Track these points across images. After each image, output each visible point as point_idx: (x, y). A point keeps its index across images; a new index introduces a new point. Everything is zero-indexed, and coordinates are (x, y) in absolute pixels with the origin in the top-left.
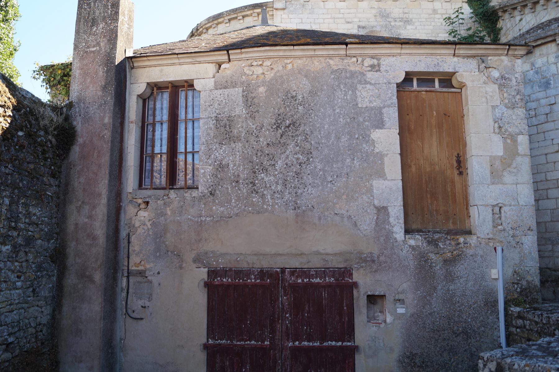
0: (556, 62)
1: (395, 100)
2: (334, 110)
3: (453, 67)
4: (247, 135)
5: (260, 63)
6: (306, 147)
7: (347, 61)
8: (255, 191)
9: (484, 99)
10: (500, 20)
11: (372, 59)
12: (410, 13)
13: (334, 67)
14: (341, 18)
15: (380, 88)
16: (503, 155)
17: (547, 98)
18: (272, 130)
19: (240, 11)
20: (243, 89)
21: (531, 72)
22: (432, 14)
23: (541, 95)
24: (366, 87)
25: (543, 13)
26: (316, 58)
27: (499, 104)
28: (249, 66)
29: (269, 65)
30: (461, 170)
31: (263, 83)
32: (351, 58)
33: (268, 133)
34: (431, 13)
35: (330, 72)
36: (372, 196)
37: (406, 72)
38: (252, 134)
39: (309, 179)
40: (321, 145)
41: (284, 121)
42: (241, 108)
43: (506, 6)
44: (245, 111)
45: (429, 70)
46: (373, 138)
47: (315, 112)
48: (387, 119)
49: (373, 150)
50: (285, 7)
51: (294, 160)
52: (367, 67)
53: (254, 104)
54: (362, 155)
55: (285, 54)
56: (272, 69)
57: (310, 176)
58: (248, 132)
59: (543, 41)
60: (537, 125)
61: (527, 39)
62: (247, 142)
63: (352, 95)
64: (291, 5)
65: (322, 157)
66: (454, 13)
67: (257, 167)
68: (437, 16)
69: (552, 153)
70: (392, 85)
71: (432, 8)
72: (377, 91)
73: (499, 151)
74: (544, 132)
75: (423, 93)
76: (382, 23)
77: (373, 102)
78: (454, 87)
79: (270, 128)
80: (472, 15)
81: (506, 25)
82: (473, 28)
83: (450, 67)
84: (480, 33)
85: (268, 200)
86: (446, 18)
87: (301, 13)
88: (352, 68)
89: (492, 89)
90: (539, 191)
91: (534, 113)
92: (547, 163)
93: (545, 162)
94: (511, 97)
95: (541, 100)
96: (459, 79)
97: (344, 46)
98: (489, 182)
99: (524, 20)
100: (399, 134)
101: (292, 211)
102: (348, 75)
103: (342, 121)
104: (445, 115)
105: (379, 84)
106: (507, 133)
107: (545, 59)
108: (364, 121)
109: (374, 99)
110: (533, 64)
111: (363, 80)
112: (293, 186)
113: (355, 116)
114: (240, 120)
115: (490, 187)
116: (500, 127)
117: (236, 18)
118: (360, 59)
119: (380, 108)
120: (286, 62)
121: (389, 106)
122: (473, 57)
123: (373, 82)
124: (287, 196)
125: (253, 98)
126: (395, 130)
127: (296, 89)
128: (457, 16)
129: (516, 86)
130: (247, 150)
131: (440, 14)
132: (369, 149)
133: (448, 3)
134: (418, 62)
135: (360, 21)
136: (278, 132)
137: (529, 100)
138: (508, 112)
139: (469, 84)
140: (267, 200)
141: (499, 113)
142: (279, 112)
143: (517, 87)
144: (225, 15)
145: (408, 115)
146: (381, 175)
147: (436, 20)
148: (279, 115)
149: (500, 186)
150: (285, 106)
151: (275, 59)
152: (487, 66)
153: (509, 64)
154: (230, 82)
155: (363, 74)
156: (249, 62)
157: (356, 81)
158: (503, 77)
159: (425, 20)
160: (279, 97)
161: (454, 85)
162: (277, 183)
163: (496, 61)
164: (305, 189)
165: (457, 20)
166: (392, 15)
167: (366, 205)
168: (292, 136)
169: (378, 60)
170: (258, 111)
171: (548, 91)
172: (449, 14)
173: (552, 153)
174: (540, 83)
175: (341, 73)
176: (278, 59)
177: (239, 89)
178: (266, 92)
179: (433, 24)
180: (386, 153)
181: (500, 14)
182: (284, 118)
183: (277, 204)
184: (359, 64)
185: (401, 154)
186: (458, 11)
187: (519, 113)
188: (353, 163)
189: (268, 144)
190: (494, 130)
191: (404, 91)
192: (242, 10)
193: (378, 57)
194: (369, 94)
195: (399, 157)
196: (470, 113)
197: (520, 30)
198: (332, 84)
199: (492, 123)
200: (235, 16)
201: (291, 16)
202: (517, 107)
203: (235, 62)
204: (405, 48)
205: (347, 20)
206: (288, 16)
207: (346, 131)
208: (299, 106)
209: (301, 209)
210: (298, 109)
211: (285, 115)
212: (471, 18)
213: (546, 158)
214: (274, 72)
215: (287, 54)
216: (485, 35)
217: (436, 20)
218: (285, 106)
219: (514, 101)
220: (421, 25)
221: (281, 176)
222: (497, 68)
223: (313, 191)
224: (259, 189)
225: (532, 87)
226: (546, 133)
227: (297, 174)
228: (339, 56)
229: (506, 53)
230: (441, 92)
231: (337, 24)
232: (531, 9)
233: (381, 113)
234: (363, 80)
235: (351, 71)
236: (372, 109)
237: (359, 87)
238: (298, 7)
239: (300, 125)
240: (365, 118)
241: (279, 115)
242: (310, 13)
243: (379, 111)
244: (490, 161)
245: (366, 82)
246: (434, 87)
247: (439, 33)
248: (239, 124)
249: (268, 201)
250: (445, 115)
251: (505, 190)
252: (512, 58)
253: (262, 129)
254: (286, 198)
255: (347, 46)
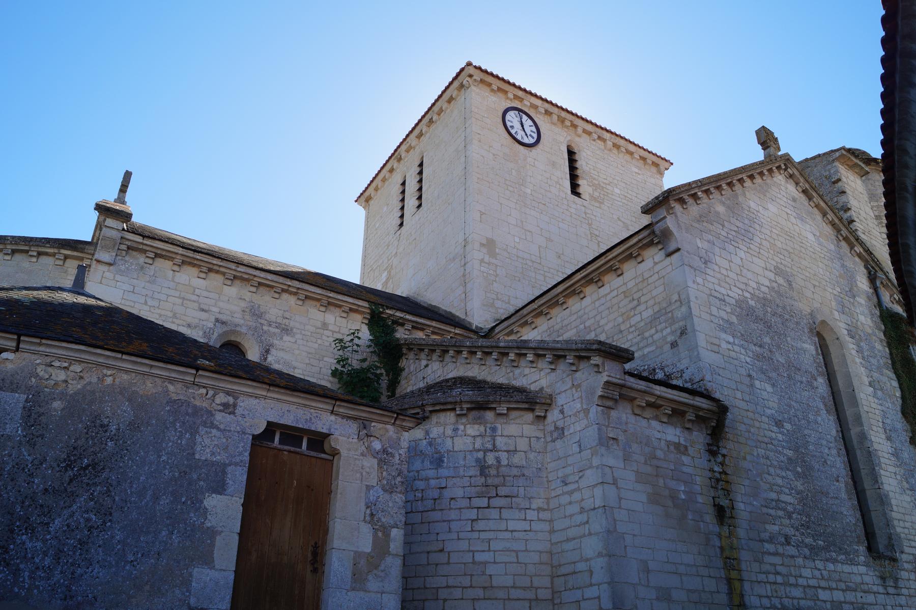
0: (453, 435)
1: (246, 457)
2: (160, 457)
3: (328, 427)
4: (15, 469)
5: (66, 365)
6: (105, 503)
7: (192, 391)
8: (5, 562)
9: (358, 475)
10: (403, 358)
11: (228, 396)
12: (293, 319)
13: (173, 395)
14: (194, 301)
15: (230, 438)
16: (371, 552)
17: (438, 479)
18: (58, 469)
19: (37, 243)
20: (28, 397)
21: (425, 442)
22: (320, 328)
23: (431, 473)
24: (211, 433)
25: (451, 366)
26: (150, 377)
27: (375, 484)
28: (46, 365)
29: (78, 371)
30: (315, 566)
31: (63, 396)
32: (199, 388)
33: (50, 472)
34: (320, 326)
35: (165, 402)
36: (188, 591)
37: (268, 422)
38: (23, 469)
39: (98, 554)
40: (129, 505)
41: (80, 458)
42: (16, 426)
43: (411, 344)
44: (21, 432)
45: (297, 426)
46: (206, 505)
47: (130, 454)
48: (231, 482)
49: (203, 523)
50: (112, 262)
51: (82, 520)
52: (219, 405)
53: (40, 425)
54: (186, 529)
55: (107, 362)
56: (81, 378)
57: (100, 550)
58: (17, 464)
59: (442, 407)
60: (422, 512)
61: (425, 400)
62: (12, 480)
63: (189, 439)
64: (123, 262)
65: (125, 523)
66: (349, 335)
67: (18, 524)
68: (327, 333)
69: (435, 552)
70: (247, 436)
71: (323, 320)
72: (224, 440)
73: (366, 545)
74: (429, 522)
75: (285, 452)
76: (251, 323)
77: (216, 454)
78: (325, 452)
79: (55, 465)
80: (370, 343)
81: (409, 367)
82: (369, 359)
83: (324, 427)
84: (376, 369)
85: (24, 579)
86: (337, 339)
87: (135, 277)
88: (198, 403)
89: (371, 463)
90: (414, 602)
91: (420, 495)
92: (428, 564)
93: (426, 563)
94: (390, 477)
95: (430, 480)
96: (333, 444)
97: (194, 372)
98: (348, 587)
99: (430, 366)
100: (243, 505)
101: (59, 602)
102: (190, 411)
103: (167, 474)
104: (309, 487)
105: (230, 431)
106: (380, 524)
107: (441, 429)
108: (199, 479)
109: (219, 450)
110: (427, 433)
111: (209, 422)
112: (70, 561)
113: (187, 470)
114: (9, 443)
115: (349, 593)
116: (372, 515)
117: (27, 252)
118: (211, 393)
119: (225, 465)
120: (105, 373)
121: (236, 464)
122: (355, 419)
123: (222, 427)
124: (57, 576)
125: (40, 415)
126: (238, 498)
127: (110, 415)
128: (352, 340)
129: (399, 464)
130: (8, 493)
131: (331, 331)
132: (197, 520)
133: (344, 319)
134: (286, 412)
135: (219, 313)
136: (67, 475)
137: (417, 478)
138: (384, 497)
139: (344, 452)
140: (21, 579)
141: (374, 496)
142: (75, 444)
143: (399, 467)
144: (9, 242)
145: (260, 479)
146: (207, 560)
147: (324, 338)
148: (74, 448)
149: (361, 594)
150: (87, 436)
151: (90, 365)
152: (369, 434)
153: (395, 436)
154: (8, 381)
155: (210, 414)
156: (48, 360)
157: (199, 421)
158: (385, 451)
159: (309, 334)
160: (81, 422)
161: (325, 449)
162: (45, 554)
163: (380, 429)
164: (88, 568)
165: (350, 344)
166: (267, 316)
167: (178, 603)
168: (88, 484)
169: (236, 398)
170: (42, 436)
171: (440, 471)
172: (343, 334)
173: (435, 552)
174: (432, 458)
175: (182, 406)
176: (94, 366)
177: (22, 395)
178: (63, 409)
179: (319, 341)
180: (220, 529)
181: (404, 351)
182: (81, 455)
183: (37, 587)
184: (209, 399)
185: (241, 535)
186: (353, 333)
187: (397, 500)
188: (171, 538)
189: (46, 490)
190: (365, 517)
191: (261, 446)
192: (41, 244)
193: (236, 394)
194: (213, 443)
195: (237, 537)
196: (339, 491)
197: (424, 378)
198: (165, 418)
199: (363, 508)
200: (26, 248)
201: (118, 277)
202: (396, 492)
203: (26, 354)
204: (273, 391)
205: (203, 306)
206: (114, 277)
207: (170, 489)
208: (108, 440)
209: (75, 599)
210: (106, 444)
211: (84, 450)
212: (369, 346)
213: (428, 558)
214: (83, 382)
215: (110, 363)
216: (381, 374)
217: (324, 338)
218: (87, 436)
219: (393, 483)
220: (303, 339)
221: (54, 542)
222: (380, 438)
223: (101, 574)
224: (13, 559)
225: (423, 462)
226: (431, 524)
227: (81, 542)
228: (183, 381)
229: (393, 422)
230: (308, 456)
231: (186, 308)
232: (440, 356)
233: (224, 473)
234: (209, 422)
235: (195, 406)
236: (213, 464)
237: (202, 430)
238: (133, 267)
239: (103, 469)
240: (200, 474)
241: (74, 448)
242: (149, 282)
243: (221, 469)
244: (354, 559)
245: (213, 426)
246: (301, 448)
247: (324, 356)
248: (5, 450)
249: (23, 582)
250: (309, 487)
251: (367, 599)
252: (399, 429)
253: (41, 464)
254: (55, 579)
255: (197, 371)
